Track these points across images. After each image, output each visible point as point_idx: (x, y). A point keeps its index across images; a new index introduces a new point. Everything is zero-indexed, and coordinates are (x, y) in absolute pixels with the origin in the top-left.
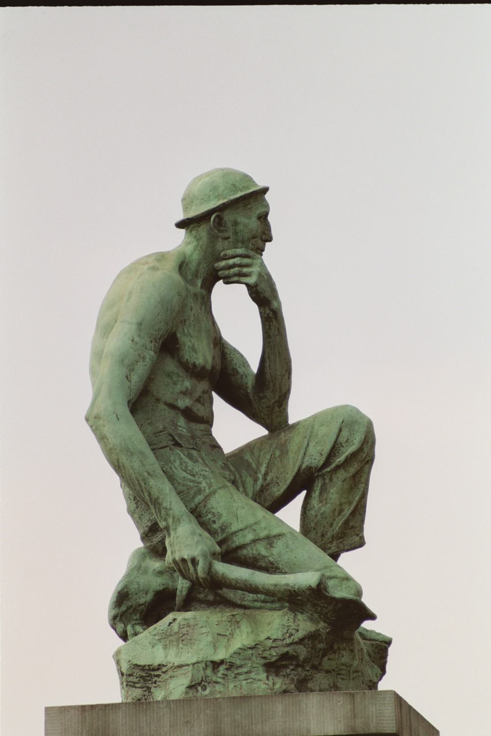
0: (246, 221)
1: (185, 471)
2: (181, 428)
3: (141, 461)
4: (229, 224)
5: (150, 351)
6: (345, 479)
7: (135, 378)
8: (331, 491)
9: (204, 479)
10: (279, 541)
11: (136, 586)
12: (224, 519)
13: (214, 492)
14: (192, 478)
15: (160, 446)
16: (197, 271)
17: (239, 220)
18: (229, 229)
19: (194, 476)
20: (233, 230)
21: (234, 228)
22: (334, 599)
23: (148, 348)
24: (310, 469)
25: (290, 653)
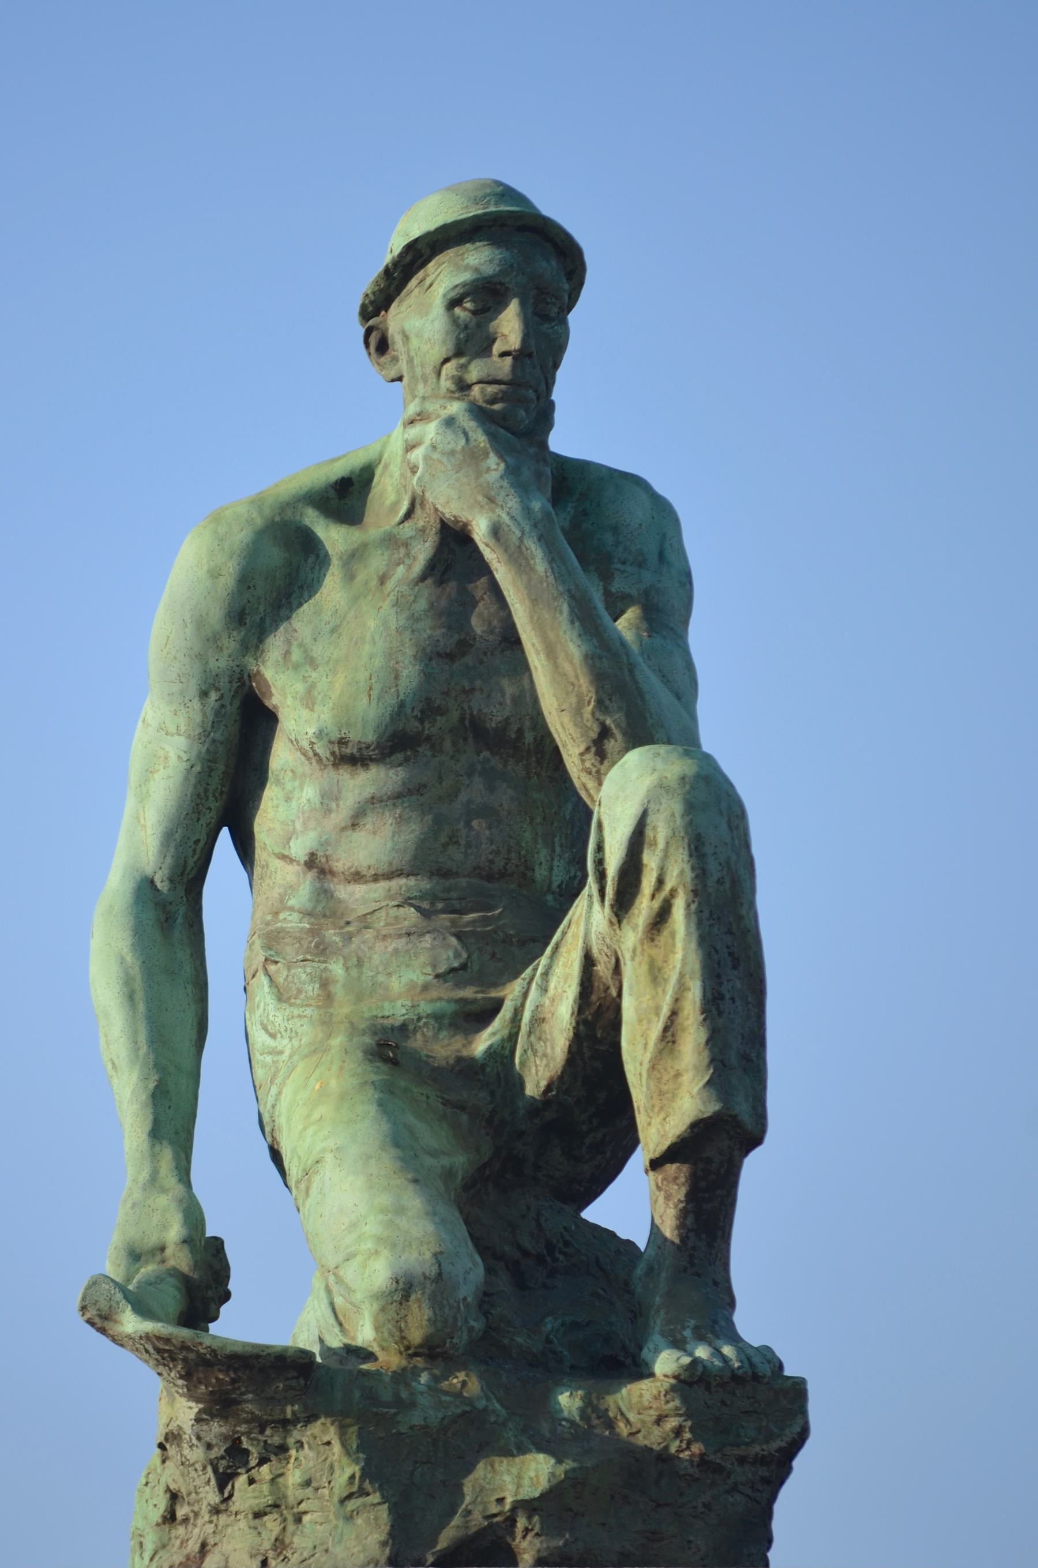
5: (176, 737)
9: (291, 1038)
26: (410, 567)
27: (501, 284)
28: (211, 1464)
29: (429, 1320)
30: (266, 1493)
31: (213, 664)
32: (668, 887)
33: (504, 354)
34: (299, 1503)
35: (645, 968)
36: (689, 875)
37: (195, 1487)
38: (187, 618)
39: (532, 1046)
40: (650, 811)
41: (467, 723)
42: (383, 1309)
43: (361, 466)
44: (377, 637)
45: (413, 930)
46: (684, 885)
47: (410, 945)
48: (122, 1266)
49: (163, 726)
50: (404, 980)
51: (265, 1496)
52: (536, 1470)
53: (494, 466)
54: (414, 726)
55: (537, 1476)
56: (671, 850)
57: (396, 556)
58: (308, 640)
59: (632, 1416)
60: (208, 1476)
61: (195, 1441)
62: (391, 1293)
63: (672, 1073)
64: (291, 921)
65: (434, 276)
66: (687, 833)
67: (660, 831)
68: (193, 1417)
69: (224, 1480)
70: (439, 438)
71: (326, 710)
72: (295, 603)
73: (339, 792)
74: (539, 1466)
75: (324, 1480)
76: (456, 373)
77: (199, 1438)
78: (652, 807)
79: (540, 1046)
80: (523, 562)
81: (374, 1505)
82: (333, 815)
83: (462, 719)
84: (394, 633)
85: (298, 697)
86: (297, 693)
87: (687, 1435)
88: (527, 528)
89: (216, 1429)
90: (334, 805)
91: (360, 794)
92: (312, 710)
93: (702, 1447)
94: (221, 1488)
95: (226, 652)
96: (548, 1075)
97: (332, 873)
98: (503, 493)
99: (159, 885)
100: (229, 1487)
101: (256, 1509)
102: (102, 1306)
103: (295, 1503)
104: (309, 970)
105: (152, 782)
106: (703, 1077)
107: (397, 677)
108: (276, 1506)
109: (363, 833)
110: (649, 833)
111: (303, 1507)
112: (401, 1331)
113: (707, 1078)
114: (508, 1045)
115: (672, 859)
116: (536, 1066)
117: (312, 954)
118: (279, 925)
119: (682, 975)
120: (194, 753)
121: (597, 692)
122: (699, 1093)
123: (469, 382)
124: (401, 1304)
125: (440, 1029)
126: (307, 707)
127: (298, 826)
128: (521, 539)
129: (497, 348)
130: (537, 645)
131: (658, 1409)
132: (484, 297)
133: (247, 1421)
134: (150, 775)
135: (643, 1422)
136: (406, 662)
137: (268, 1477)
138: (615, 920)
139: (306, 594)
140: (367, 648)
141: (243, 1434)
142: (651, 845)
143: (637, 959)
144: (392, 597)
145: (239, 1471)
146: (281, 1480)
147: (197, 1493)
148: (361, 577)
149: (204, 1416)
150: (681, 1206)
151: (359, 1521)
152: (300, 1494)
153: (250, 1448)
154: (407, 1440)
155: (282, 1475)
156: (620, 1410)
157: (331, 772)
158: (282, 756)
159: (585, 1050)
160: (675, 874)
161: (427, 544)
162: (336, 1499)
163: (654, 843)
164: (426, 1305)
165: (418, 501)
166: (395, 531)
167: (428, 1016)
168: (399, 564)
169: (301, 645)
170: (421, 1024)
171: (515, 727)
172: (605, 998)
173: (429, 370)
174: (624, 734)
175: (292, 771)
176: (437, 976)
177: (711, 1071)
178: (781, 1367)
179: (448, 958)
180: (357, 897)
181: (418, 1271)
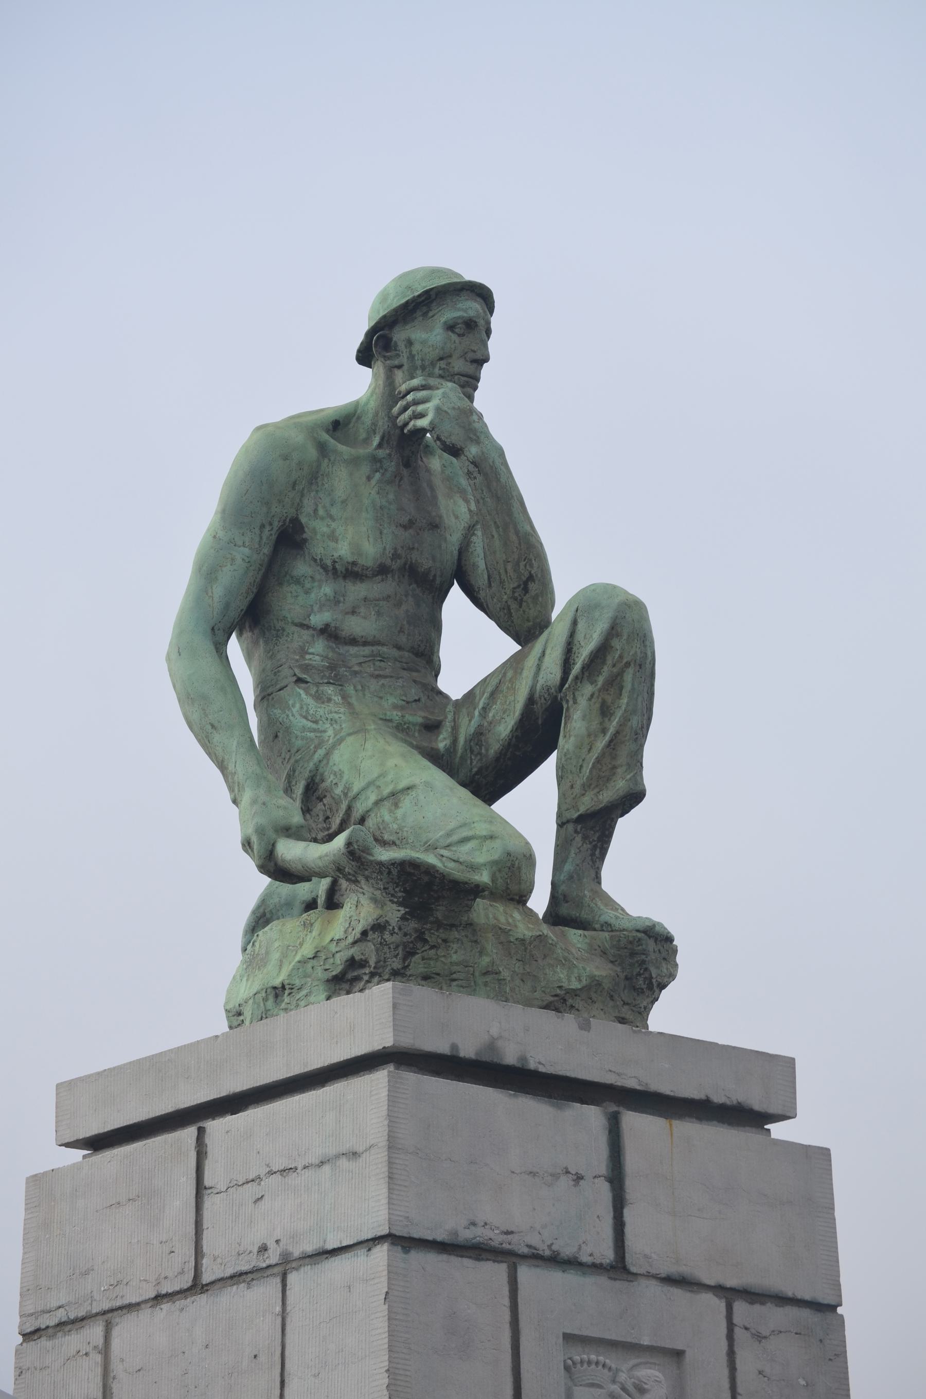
0: (424, 336)
1: (306, 718)
2: (311, 656)
3: (204, 710)
4: (402, 346)
5: (242, 548)
6: (592, 696)
7: (218, 591)
8: (575, 717)
9: (332, 725)
10: (407, 797)
11: (277, 900)
12: (346, 777)
13: (341, 741)
14: (314, 726)
15: (278, 687)
16: (374, 424)
17: (413, 337)
19: (316, 722)
22: (381, 864)
24: (548, 690)
25: (357, 958)
27: (476, 322)
35: (598, 705)
50: (390, 702)
54: (388, 562)
61: (396, 930)
63: (610, 766)
69: (410, 954)
77: (400, 929)
83: (405, 564)
89: (413, 925)
90: (342, 599)
94: (404, 960)
96: (479, 765)
111: (454, 976)
116: (471, 759)
133: (432, 923)
140: (364, 515)
143: (593, 700)
144: (376, 489)
169: (324, 507)
171: (433, 573)
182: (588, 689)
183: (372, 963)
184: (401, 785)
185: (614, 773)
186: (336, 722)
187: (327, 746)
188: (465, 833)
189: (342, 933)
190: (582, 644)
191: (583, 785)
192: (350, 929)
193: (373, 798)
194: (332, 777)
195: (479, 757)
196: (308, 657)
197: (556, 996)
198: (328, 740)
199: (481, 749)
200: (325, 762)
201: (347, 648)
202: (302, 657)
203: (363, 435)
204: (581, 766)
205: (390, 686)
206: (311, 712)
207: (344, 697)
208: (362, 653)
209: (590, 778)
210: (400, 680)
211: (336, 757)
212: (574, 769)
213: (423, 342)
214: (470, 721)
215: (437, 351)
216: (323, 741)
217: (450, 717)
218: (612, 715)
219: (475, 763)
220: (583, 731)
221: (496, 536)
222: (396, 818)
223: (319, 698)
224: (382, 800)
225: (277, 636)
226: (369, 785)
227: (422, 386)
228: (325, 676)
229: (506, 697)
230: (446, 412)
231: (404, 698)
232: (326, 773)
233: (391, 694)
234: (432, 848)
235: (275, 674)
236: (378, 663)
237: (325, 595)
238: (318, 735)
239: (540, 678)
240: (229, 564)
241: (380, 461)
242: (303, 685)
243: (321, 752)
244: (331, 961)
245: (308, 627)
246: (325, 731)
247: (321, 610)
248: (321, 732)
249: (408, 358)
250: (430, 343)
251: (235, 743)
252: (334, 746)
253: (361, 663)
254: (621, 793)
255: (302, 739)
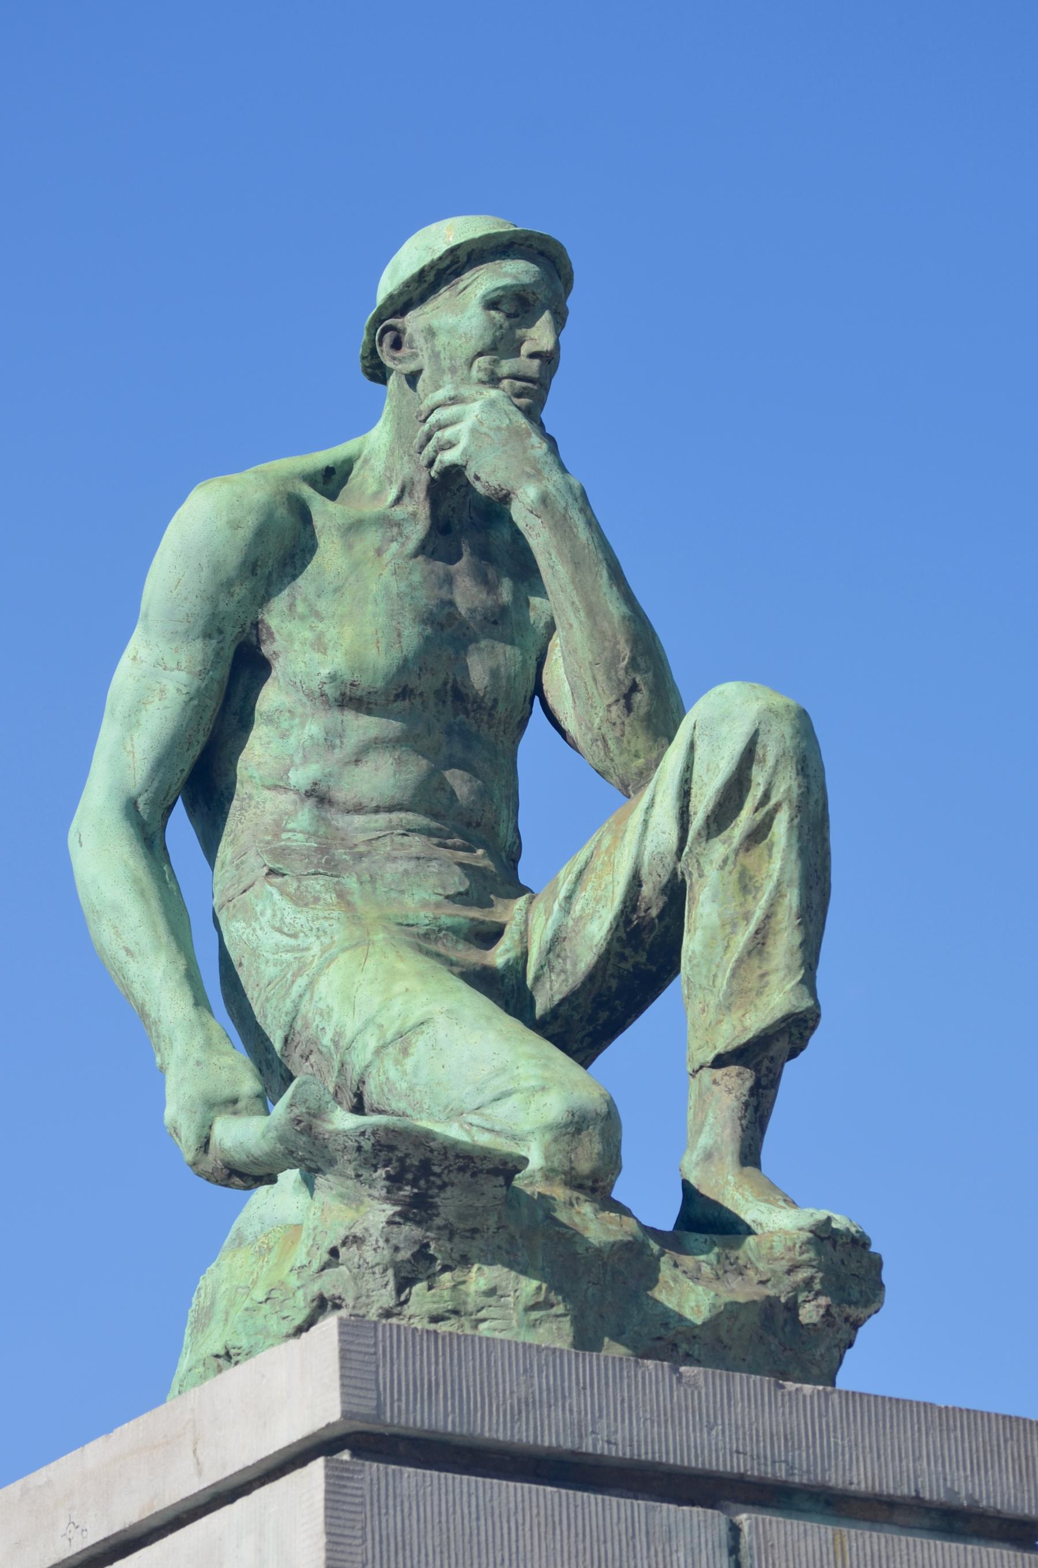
1: (280, 930)
2: (290, 835)
4: (420, 341)
5: (176, 672)
6: (725, 861)
8: (702, 898)
9: (318, 937)
10: (421, 1038)
14: (292, 942)
15: (242, 886)
17: (435, 323)
18: (422, 350)
19: (294, 936)
20: (429, 351)
21: (429, 345)
23: (169, 666)
24: (661, 860)
26: (403, 544)
28: (394, 1268)
29: (598, 1154)
30: (447, 1298)
31: (222, 607)
32: (773, 801)
33: (532, 356)
34: (479, 1311)
35: (735, 876)
36: (796, 791)
37: (368, 1290)
38: (204, 562)
39: (549, 962)
40: (761, 732)
41: (449, 686)
42: (556, 1140)
43: (342, 458)
44: (379, 599)
45: (422, 855)
46: (790, 801)
47: (420, 868)
48: (198, 1115)
49: (161, 662)
51: (446, 1301)
52: (697, 1301)
53: (537, 445)
55: (698, 1306)
56: (780, 768)
57: (389, 534)
58: (312, 596)
59: (761, 1266)
60: (386, 1279)
61: (381, 1243)
62: (566, 1125)
64: (296, 841)
65: (470, 281)
66: (795, 753)
67: (771, 750)
68: (384, 1219)
69: (404, 1284)
70: (484, 416)
71: (339, 654)
72: (299, 563)
73: (343, 731)
74: (700, 1298)
75: (510, 1288)
76: (489, 366)
77: (387, 1241)
78: (763, 727)
79: (558, 964)
80: (568, 530)
81: (557, 1316)
82: (337, 751)
84: (395, 597)
85: (308, 642)
86: (306, 639)
87: (817, 1286)
88: (570, 501)
90: (338, 742)
91: (364, 734)
92: (325, 654)
93: (829, 1299)
94: (399, 1291)
95: (236, 598)
97: (331, 803)
98: (547, 469)
99: (141, 807)
100: (407, 1291)
101: (435, 1313)
102: (312, 1105)
103: (475, 1309)
104: (321, 882)
105: (144, 713)
106: (795, 976)
107: (399, 635)
108: (456, 1312)
109: (365, 769)
110: (760, 751)
111: (482, 1314)
112: (571, 1162)
113: (799, 977)
114: (521, 962)
115: (780, 776)
117: (324, 868)
118: (283, 843)
119: (779, 883)
120: (195, 686)
121: (631, 651)
122: (792, 990)
123: (500, 375)
124: (573, 1135)
125: (457, 941)
126: (319, 651)
127: (297, 759)
128: (566, 509)
129: (525, 349)
130: (577, 603)
131: (791, 1259)
132: (516, 307)
134: (143, 706)
135: (774, 1272)
136: (407, 623)
137: (449, 1285)
138: (704, 833)
139: (308, 556)
140: (370, 607)
141: (432, 1239)
142: (760, 762)
143: (728, 868)
144: (390, 567)
145: (420, 1276)
146: (462, 1287)
147: (368, 1296)
148: (359, 547)
149: (397, 1219)
150: (743, 1099)
151: (541, 1330)
152: (482, 1300)
153: (436, 1255)
154: (583, 1261)
155: (464, 1282)
156: (750, 1259)
157: (336, 715)
158: (270, 697)
159: (610, 966)
160: (782, 790)
161: (419, 527)
162: (521, 1307)
163: (764, 760)
164: (596, 1138)
165: (407, 490)
166: (388, 512)
167: (448, 929)
168: (392, 541)
169: (305, 600)
170: (441, 935)
172: (644, 917)
173: (460, 362)
174: (651, 692)
175: (290, 711)
176: (447, 897)
177: (803, 972)
178: (869, 1245)
179: (454, 884)
180: (359, 826)
181: (591, 1107)
182: (719, 849)
183: (349, 1301)
184: (411, 1022)
185: (767, 984)
186: (325, 932)
187: (311, 971)
188: (501, 1084)
189: (304, 1256)
190: (705, 779)
191: (719, 1006)
192: (315, 1248)
193: (373, 1043)
194: (318, 1019)
195: (563, 977)
196: (284, 836)
197: (659, 1338)
198: (312, 962)
199: (565, 963)
200: (307, 997)
201: (348, 818)
202: (277, 836)
203: (372, 487)
204: (715, 976)
205: (417, 874)
206: (288, 920)
207: (342, 895)
208: (373, 825)
209: (730, 994)
210: (434, 863)
211: (322, 986)
212: (704, 982)
213: (451, 331)
214: (547, 920)
215: (473, 342)
216: (305, 965)
217: (518, 917)
218: (757, 889)
219: (556, 986)
220: (715, 920)
221: (576, 625)
222: (405, 1073)
223: (299, 900)
224: (384, 1046)
225: (242, 809)
226: (368, 1022)
227: (450, 399)
228: (311, 863)
229: (600, 877)
230: (485, 434)
231: (440, 891)
232: (310, 1015)
233: (419, 886)
234: (456, 1114)
235: (237, 867)
236: (399, 839)
237: (311, 737)
238: (298, 955)
239: (647, 843)
240: (156, 699)
241: (398, 525)
242: (278, 880)
243: (302, 981)
244: (291, 1303)
245: (286, 789)
246: (307, 949)
247: (305, 760)
248: (303, 950)
249: (430, 358)
250: (461, 331)
251: (160, 974)
252: (319, 973)
253: (370, 840)
254: (778, 1015)
255: (275, 965)
